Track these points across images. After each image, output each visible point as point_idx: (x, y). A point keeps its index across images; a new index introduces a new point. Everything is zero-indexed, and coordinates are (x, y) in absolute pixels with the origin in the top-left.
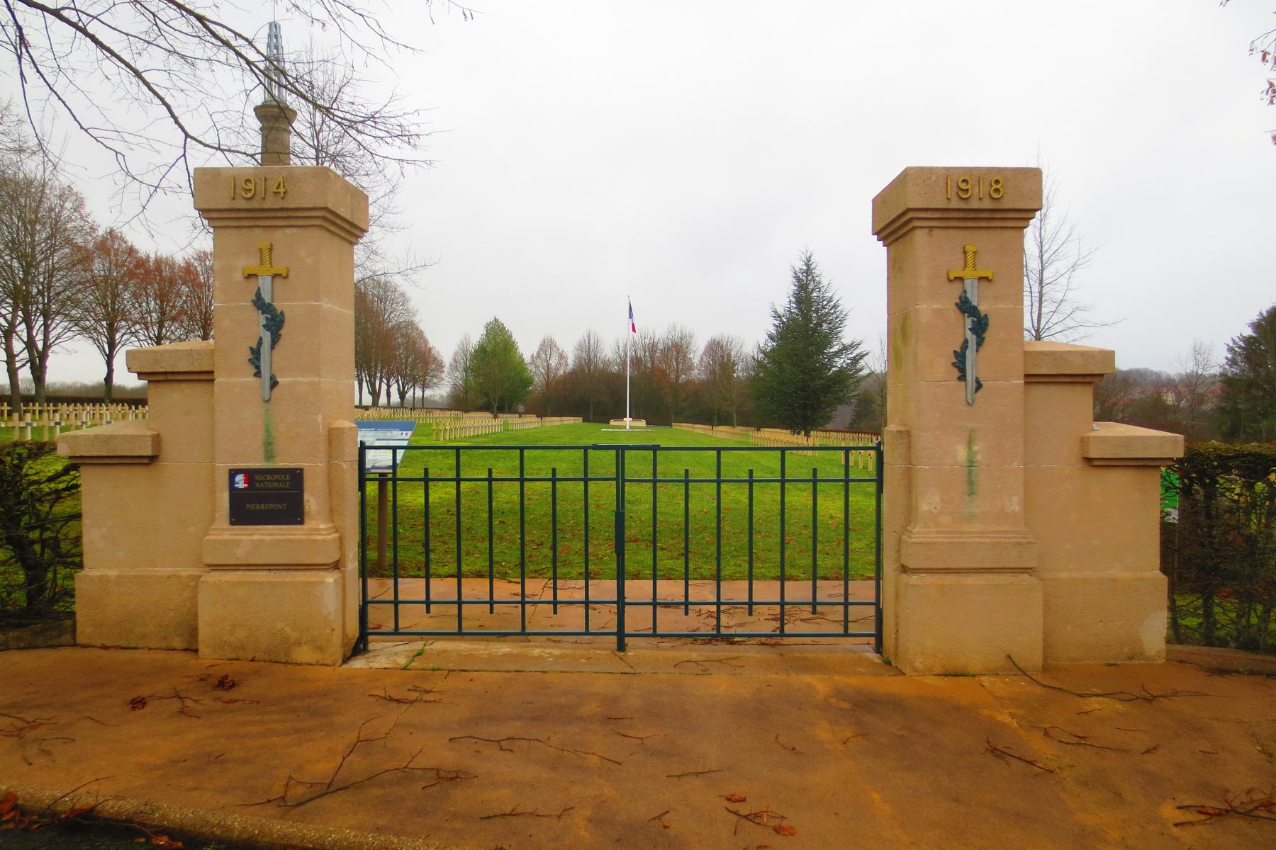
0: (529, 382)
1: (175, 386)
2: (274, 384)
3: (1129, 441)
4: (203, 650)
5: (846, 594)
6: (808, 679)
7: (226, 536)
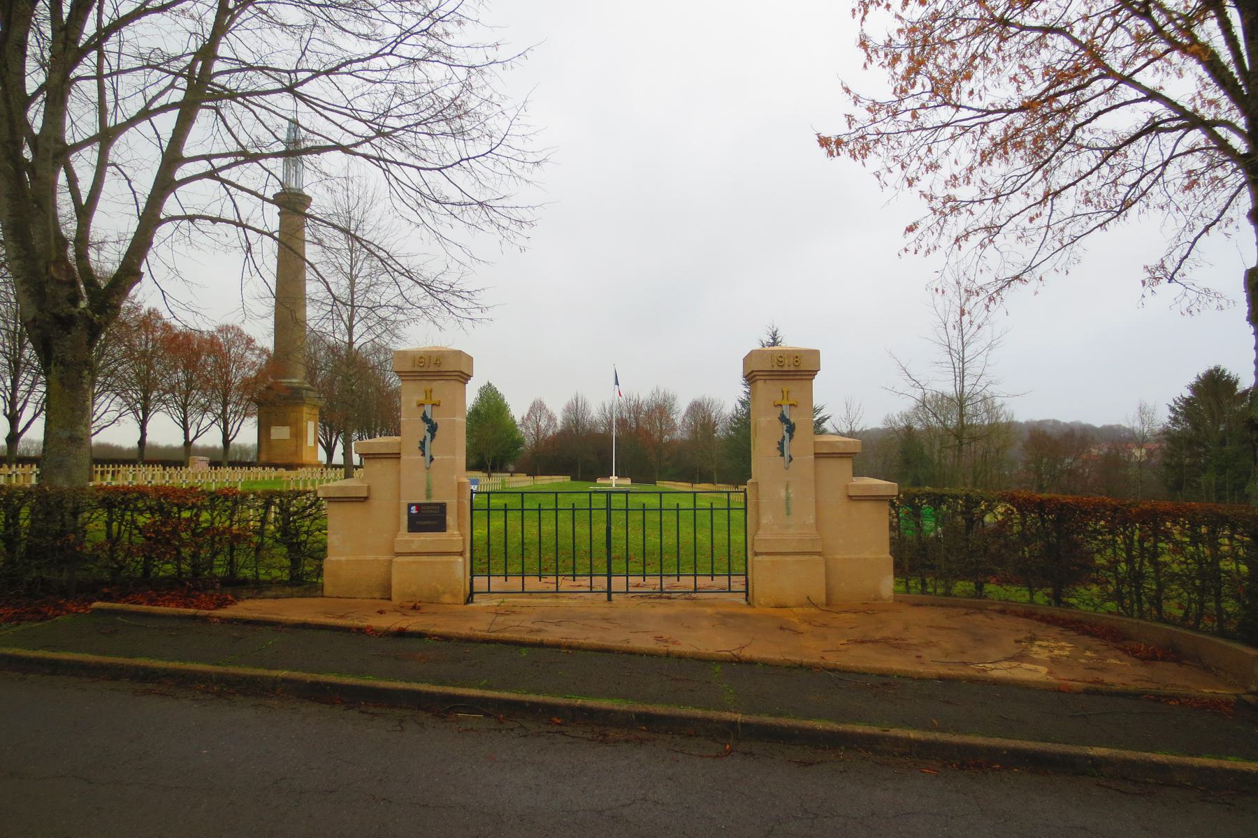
0: (520, 442)
1: (378, 460)
2: (432, 459)
3: (870, 487)
4: (394, 597)
5: (729, 570)
6: (704, 609)
7: (406, 538)
